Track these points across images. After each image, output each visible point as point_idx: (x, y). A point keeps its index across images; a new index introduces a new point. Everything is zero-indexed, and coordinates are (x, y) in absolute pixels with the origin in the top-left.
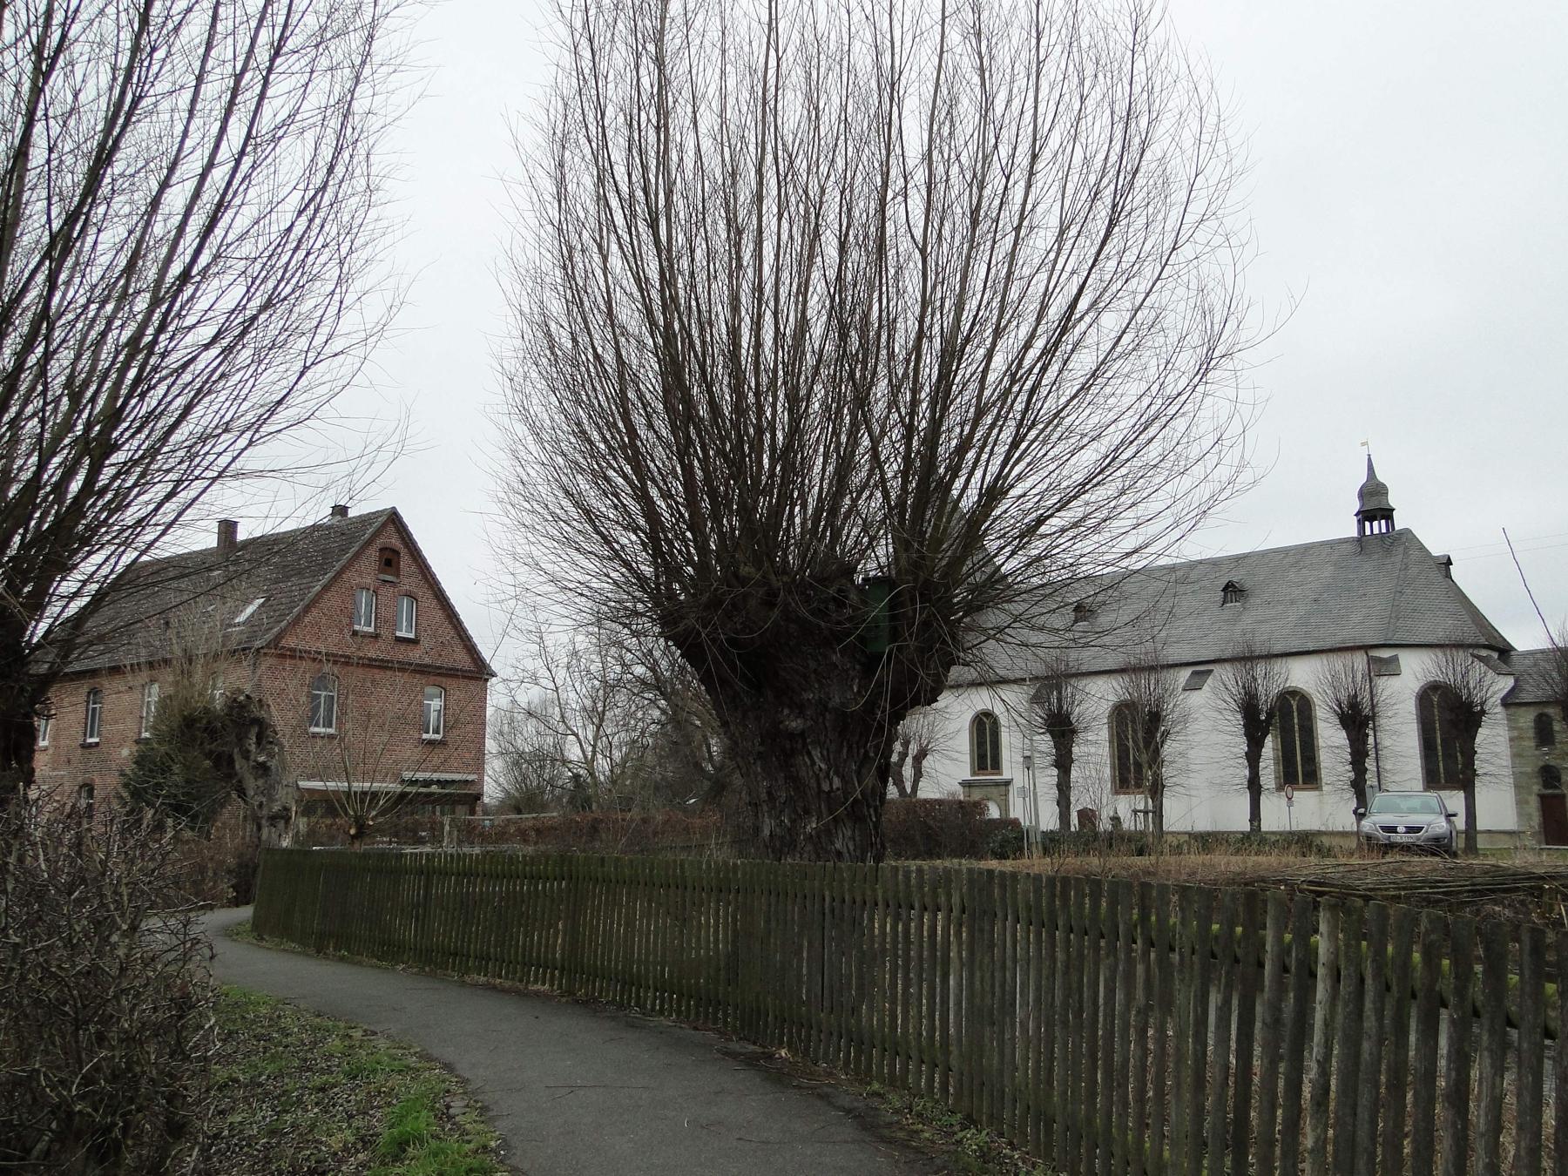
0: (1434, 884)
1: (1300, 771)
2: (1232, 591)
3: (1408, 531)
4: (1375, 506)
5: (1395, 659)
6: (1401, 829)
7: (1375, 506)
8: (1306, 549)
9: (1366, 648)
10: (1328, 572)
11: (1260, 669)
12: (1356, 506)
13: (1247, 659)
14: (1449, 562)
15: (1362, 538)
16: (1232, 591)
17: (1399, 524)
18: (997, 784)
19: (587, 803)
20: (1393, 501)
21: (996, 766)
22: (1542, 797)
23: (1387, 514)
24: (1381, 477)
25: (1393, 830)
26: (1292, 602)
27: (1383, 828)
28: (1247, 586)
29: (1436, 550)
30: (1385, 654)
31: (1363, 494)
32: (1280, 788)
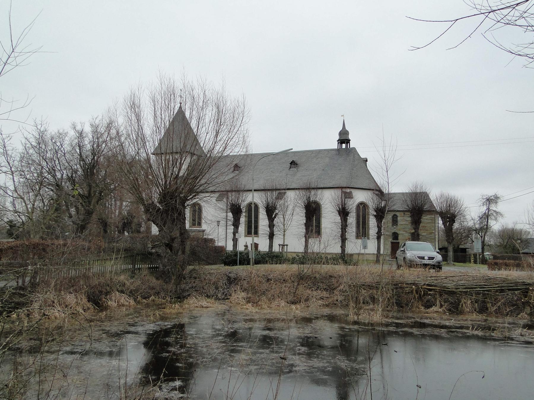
0: (481, 287)
1: (252, 229)
2: (293, 164)
3: (354, 148)
4: (344, 139)
5: (351, 192)
6: (426, 258)
7: (344, 139)
8: (320, 151)
9: (342, 188)
10: (327, 160)
11: (313, 192)
12: (338, 138)
13: (308, 189)
14: (367, 161)
15: (339, 150)
16: (293, 164)
17: (352, 145)
18: (199, 231)
19: (119, 371)
20: (350, 137)
21: (200, 224)
22: (392, 243)
23: (347, 141)
24: (347, 128)
25: (423, 258)
26: (315, 170)
27: (419, 257)
28: (298, 163)
29: (363, 156)
30: (348, 190)
31: (341, 134)
32: (358, 237)
